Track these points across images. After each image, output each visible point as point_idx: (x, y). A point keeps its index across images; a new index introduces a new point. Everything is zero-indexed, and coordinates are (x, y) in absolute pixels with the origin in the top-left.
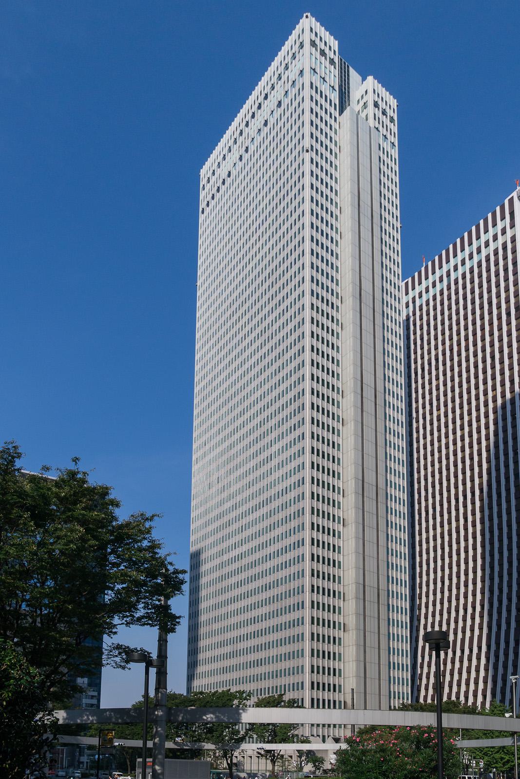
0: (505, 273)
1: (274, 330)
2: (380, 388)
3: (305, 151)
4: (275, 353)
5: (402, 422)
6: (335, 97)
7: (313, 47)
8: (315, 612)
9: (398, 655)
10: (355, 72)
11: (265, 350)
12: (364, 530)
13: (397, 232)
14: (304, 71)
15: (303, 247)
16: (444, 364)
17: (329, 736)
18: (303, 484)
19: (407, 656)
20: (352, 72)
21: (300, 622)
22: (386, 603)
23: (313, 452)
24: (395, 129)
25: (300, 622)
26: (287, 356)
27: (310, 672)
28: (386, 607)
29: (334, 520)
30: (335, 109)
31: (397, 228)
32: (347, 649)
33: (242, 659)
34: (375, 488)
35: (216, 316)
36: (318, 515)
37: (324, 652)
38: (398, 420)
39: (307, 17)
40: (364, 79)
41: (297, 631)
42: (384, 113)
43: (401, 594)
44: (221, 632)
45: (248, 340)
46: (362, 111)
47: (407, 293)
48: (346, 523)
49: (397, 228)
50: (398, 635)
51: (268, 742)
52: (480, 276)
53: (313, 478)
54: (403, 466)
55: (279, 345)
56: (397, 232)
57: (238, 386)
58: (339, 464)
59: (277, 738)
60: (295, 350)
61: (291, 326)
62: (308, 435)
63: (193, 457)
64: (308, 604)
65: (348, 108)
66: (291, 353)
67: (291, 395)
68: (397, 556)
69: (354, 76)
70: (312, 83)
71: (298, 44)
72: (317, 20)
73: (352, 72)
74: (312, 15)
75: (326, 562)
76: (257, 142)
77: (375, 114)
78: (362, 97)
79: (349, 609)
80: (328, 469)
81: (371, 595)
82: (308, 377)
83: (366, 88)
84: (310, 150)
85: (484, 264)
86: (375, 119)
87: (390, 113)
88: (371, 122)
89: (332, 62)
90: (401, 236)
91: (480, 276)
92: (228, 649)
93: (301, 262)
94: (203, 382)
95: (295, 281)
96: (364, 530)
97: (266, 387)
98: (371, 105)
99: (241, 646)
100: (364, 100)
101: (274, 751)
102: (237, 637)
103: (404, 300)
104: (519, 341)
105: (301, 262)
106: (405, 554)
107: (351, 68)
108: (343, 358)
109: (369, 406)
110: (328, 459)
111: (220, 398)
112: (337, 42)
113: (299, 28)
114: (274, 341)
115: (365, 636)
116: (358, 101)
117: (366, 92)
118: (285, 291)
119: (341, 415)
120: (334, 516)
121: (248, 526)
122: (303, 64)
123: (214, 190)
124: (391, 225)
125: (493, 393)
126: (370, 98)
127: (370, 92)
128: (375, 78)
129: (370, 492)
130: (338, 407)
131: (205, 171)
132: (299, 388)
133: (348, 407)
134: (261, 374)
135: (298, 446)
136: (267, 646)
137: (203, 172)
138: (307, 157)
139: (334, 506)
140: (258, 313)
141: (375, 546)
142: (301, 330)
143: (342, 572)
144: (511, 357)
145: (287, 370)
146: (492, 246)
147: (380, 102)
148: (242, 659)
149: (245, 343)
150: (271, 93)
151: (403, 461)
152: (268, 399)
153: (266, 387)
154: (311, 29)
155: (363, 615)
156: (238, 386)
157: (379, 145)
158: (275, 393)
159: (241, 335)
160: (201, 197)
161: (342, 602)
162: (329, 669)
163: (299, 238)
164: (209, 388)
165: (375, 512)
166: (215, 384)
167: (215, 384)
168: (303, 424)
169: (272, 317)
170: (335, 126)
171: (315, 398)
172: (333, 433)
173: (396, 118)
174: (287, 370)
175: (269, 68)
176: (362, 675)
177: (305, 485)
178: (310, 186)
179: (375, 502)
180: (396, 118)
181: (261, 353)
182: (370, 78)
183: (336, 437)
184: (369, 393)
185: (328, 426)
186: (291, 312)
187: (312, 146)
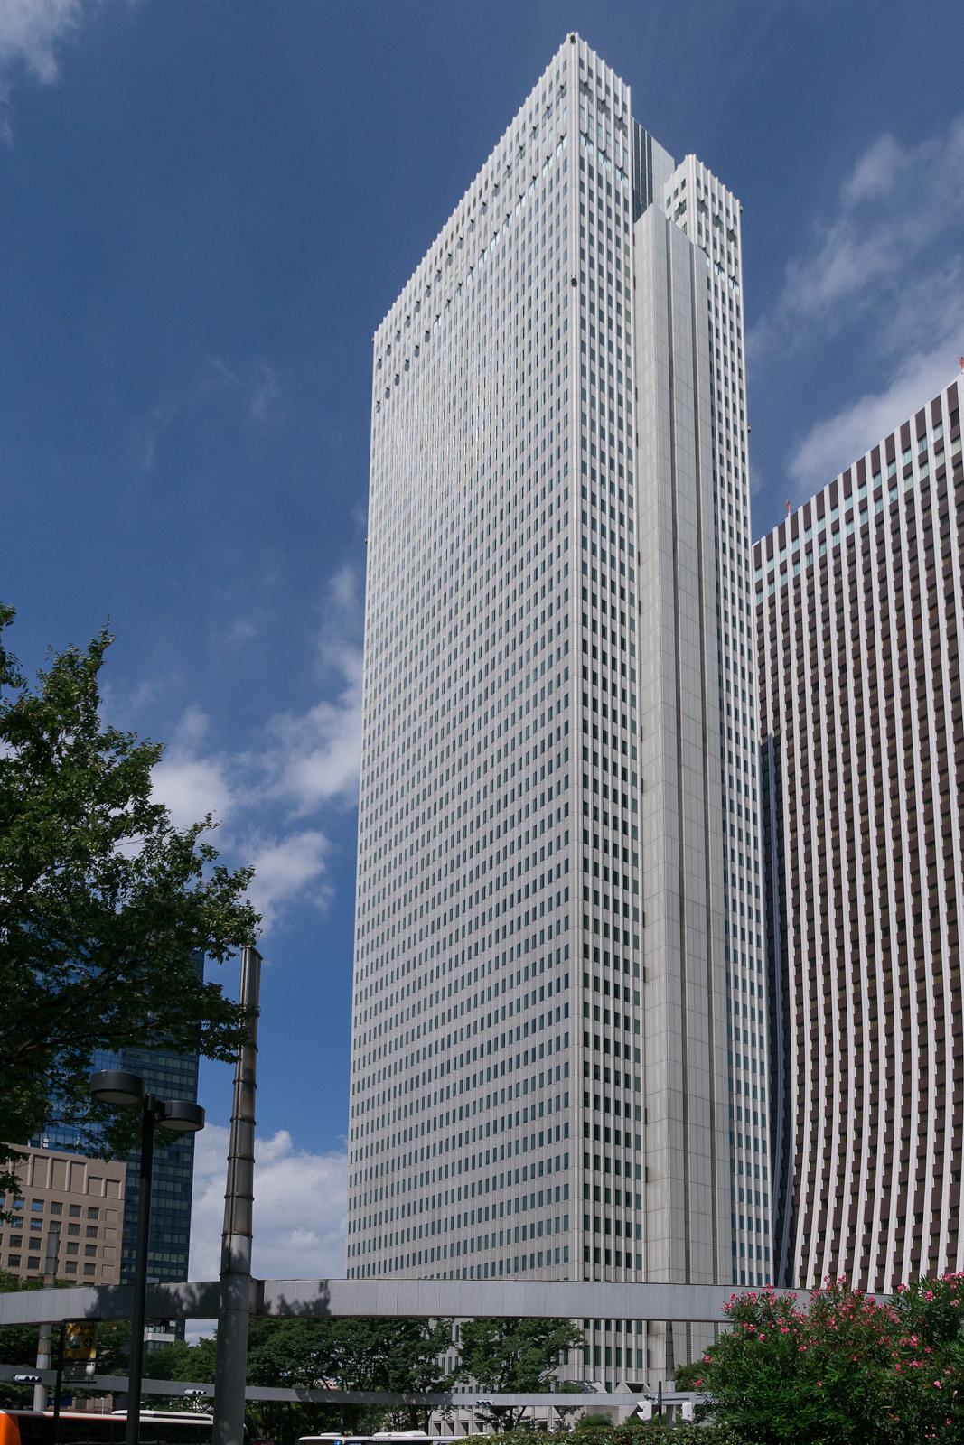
0: (942, 524)
1: (511, 614)
2: (712, 722)
3: (569, 282)
4: (513, 657)
5: (753, 767)
6: (626, 186)
7: (584, 94)
8: (591, 1143)
9: (750, 1228)
10: (660, 146)
11: (494, 652)
12: (683, 990)
13: (742, 439)
14: (568, 86)
15: (566, 245)
16: (830, 694)
17: (617, 1384)
18: (567, 957)
19: (766, 1204)
20: (657, 148)
21: (562, 1163)
22: (727, 1129)
23: (585, 841)
24: (737, 252)
25: (563, 1101)
26: (536, 662)
27: (581, 1260)
28: (727, 1137)
29: (626, 999)
30: (626, 209)
31: (742, 433)
32: (651, 1216)
33: (450, 1237)
34: (708, 1104)
35: (402, 596)
36: (596, 1017)
37: (607, 1221)
38: (746, 786)
39: (573, 39)
40: (679, 160)
41: (556, 1180)
42: (717, 221)
43: (753, 1035)
44: (403, 1209)
45: (462, 637)
46: (677, 219)
47: (758, 567)
48: (649, 975)
49: (742, 433)
50: (750, 1246)
51: (501, 1391)
52: (896, 531)
53: (585, 861)
54: (755, 823)
55: (521, 642)
56: (742, 439)
57: (443, 723)
58: (635, 864)
59: (516, 1384)
60: (551, 648)
61: (543, 605)
62: (576, 809)
63: (356, 923)
64: (576, 1129)
65: (650, 208)
66: (543, 656)
67: (543, 734)
68: (745, 1041)
69: (660, 154)
70: (582, 160)
71: (556, 89)
72: (592, 46)
73: (657, 148)
74: (583, 37)
75: (612, 1049)
76: (479, 274)
77: (699, 224)
78: (676, 193)
79: (658, 1138)
80: (616, 874)
81: (698, 1113)
82: (576, 698)
83: (682, 177)
84: (578, 281)
85: (903, 509)
86: (700, 232)
87: (728, 223)
88: (693, 235)
89: (620, 122)
90: (749, 450)
91: (896, 531)
92: (423, 1218)
93: (562, 511)
94: (374, 825)
95: (551, 522)
96: (683, 990)
97: (496, 721)
98: (692, 207)
99: (449, 1211)
100: (680, 199)
101: (511, 1408)
102: (440, 1195)
103: (753, 577)
104: (962, 525)
105: (562, 511)
106: (764, 1142)
107: (654, 141)
108: (645, 848)
109: (692, 756)
110: (615, 854)
111: (409, 746)
112: (628, 89)
113: (557, 60)
114: (511, 635)
115: (686, 1192)
116: (669, 201)
117: (683, 184)
118: (532, 566)
119: (638, 773)
120: (626, 990)
121: (450, 1224)
122: (565, 127)
123: (400, 368)
124: (729, 363)
125: (904, 460)
126: (690, 195)
127: (691, 182)
128: (699, 159)
129: (695, 918)
130: (634, 757)
131: (381, 336)
132: (559, 720)
133: (652, 755)
134: (487, 698)
135: (558, 830)
136: (499, 1211)
137: (378, 336)
138: (574, 293)
139: (626, 999)
140: (481, 633)
141: (706, 1019)
142: (562, 612)
143: (641, 1039)
144: (947, 555)
145: (535, 688)
146: (918, 475)
147: (709, 203)
148: (450, 1237)
149: (456, 642)
150: (504, 183)
151: (758, 912)
152: (499, 743)
153: (496, 721)
154: (581, 63)
155: (684, 1150)
156: (443, 723)
157: (709, 280)
158: (512, 784)
159: (450, 627)
160: (375, 382)
161: (642, 1126)
162: (617, 1162)
163: (558, 515)
164: (388, 731)
165: (705, 983)
166: (399, 721)
167: (399, 721)
168: (567, 759)
169: (508, 591)
170: (627, 240)
171: (590, 739)
172: (625, 859)
173: (738, 233)
174: (535, 688)
175: (508, 129)
176: (682, 1265)
177: (570, 960)
178: (578, 299)
179: (704, 937)
180: (738, 233)
181: (487, 658)
182: (691, 159)
183: (629, 813)
184: (691, 732)
185: (615, 792)
186: (543, 579)
187: (582, 274)
